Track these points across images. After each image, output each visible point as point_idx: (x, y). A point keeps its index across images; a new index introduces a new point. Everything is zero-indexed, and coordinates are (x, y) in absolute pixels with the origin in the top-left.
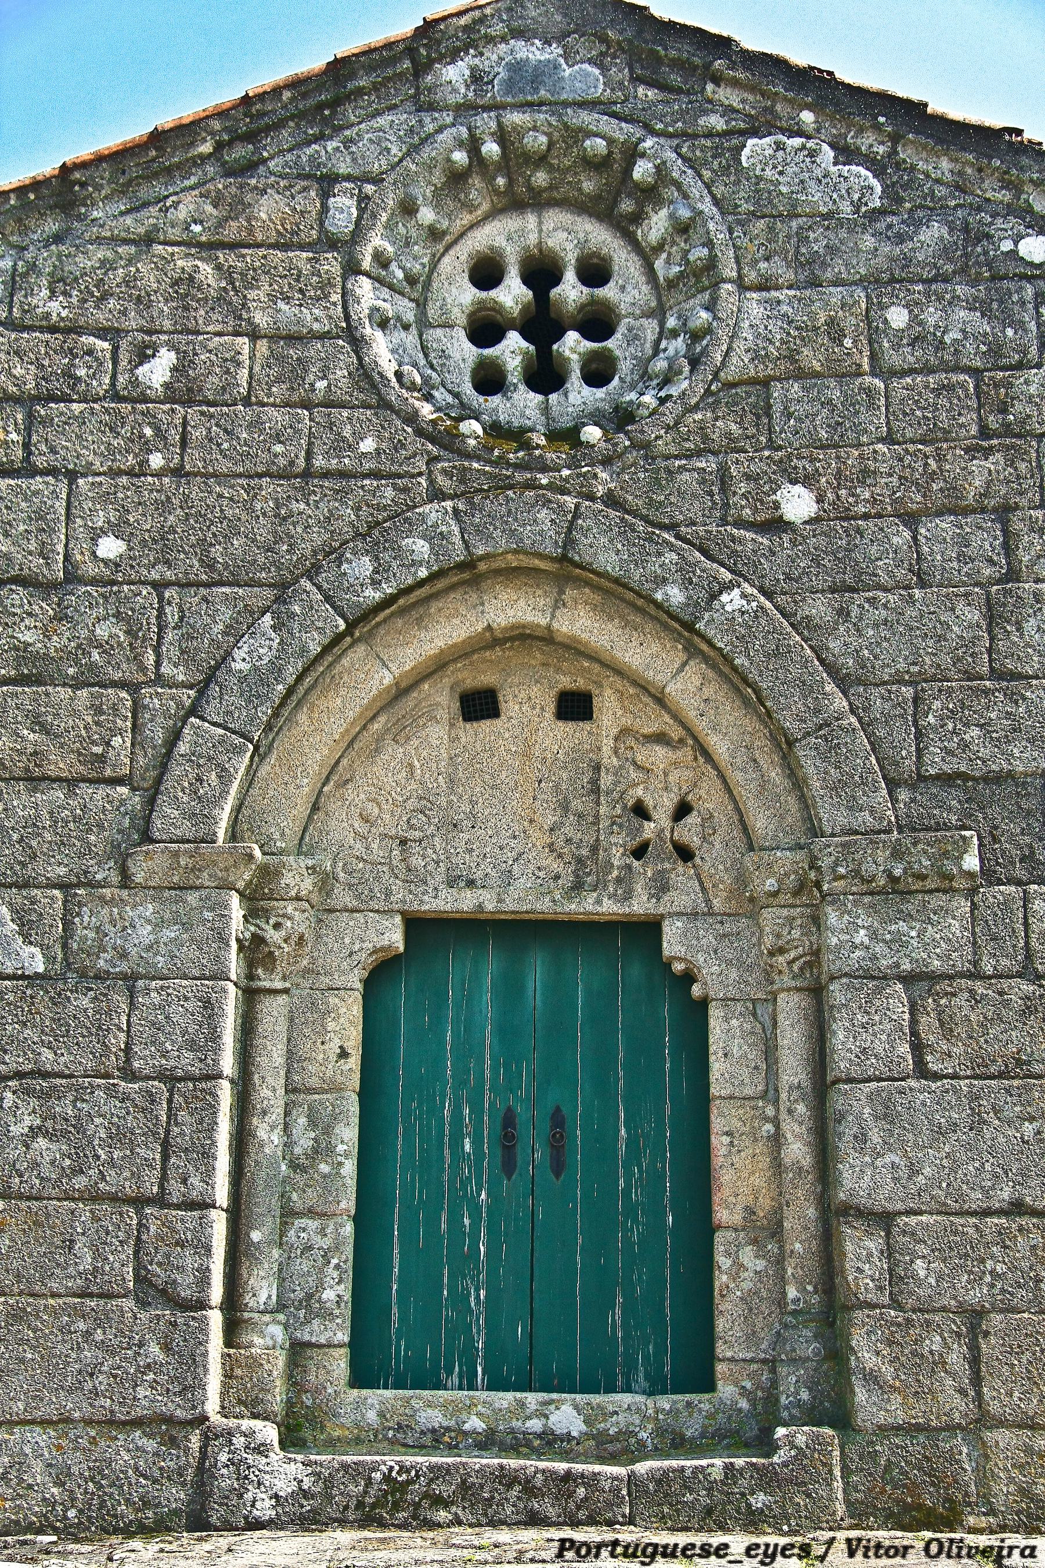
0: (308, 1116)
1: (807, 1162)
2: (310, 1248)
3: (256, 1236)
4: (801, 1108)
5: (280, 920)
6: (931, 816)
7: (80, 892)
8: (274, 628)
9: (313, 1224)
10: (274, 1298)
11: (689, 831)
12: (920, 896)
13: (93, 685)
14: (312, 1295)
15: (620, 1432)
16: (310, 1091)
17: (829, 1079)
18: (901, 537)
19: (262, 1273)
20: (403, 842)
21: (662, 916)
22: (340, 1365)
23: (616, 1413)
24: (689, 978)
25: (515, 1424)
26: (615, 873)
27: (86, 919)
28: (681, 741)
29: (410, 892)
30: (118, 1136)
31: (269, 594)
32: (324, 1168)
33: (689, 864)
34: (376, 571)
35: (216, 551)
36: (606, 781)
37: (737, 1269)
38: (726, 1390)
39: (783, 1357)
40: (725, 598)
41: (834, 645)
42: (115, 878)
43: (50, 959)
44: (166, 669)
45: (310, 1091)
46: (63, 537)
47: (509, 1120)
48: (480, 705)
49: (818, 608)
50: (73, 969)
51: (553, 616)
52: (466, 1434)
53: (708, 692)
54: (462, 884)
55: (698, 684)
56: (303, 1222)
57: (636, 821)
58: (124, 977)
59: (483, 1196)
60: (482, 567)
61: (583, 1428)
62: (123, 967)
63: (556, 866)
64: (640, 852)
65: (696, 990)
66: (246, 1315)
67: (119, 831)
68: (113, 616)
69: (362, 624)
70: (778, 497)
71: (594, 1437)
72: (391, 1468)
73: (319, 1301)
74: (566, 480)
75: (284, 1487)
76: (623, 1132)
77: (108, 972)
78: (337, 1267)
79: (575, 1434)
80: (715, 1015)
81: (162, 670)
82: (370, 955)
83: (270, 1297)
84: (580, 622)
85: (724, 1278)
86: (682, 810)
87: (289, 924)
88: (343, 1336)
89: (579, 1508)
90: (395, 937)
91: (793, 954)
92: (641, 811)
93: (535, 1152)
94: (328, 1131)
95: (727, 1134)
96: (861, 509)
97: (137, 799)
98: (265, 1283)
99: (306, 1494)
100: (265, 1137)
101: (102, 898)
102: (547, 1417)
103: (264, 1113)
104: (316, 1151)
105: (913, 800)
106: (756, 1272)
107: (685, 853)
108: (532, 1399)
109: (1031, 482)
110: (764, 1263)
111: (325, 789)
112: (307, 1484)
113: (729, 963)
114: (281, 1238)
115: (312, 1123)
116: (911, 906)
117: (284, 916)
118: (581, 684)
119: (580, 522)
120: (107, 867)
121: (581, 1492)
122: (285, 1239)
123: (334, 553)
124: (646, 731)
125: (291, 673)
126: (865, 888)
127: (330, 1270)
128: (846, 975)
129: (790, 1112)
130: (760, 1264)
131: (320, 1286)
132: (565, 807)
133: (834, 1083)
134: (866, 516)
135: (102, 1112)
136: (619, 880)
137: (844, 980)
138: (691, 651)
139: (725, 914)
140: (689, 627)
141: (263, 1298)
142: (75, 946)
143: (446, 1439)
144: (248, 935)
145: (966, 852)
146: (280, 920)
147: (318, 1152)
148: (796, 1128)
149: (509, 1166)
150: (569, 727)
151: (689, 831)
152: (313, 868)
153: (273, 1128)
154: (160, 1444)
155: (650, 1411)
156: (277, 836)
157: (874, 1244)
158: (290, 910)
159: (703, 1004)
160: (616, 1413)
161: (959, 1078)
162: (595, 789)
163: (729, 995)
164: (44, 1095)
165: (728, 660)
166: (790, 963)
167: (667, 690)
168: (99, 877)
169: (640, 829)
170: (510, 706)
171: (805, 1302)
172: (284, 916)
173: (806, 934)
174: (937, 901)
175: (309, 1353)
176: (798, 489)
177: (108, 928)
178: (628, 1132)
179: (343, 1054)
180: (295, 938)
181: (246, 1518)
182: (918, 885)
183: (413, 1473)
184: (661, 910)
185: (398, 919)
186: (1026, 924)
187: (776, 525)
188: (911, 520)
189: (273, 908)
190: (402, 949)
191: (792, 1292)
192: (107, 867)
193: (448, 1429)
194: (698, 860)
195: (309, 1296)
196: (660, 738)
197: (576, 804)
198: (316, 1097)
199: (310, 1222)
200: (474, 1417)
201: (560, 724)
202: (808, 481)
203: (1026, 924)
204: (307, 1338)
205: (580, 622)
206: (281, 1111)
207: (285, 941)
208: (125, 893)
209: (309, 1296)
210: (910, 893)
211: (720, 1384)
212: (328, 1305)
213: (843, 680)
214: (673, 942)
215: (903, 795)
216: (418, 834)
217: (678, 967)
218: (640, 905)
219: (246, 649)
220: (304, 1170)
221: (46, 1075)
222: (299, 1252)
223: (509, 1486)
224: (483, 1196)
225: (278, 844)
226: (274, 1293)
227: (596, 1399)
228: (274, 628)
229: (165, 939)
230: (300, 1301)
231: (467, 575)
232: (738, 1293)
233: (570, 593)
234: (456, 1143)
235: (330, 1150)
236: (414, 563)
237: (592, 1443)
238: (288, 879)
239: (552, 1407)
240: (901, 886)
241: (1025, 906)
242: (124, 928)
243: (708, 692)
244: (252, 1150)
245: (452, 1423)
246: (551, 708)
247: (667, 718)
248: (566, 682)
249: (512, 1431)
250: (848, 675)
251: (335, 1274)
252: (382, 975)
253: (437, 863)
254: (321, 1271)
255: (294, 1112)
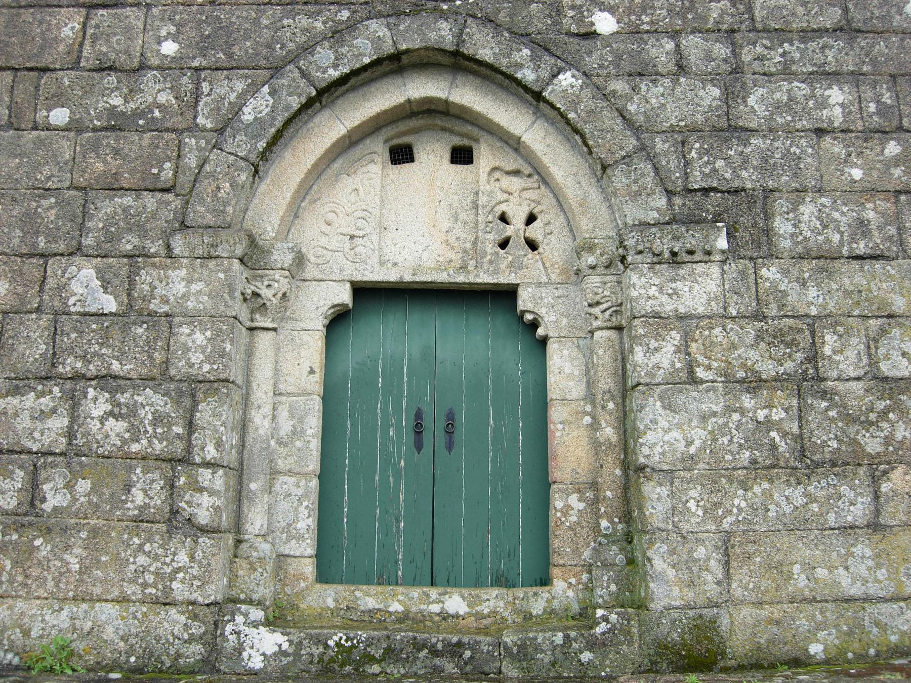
0: (289, 411)
1: (614, 439)
2: (290, 495)
3: (253, 486)
4: (611, 405)
5: (270, 282)
6: (694, 215)
7: (140, 260)
8: (270, 94)
9: (291, 480)
10: (265, 526)
11: (536, 231)
12: (690, 265)
13: (154, 131)
14: (291, 525)
15: (490, 612)
16: (289, 394)
17: (630, 383)
18: (670, 46)
19: (257, 510)
20: (352, 237)
21: (518, 285)
22: (309, 568)
23: (488, 600)
24: (534, 325)
25: (423, 607)
26: (489, 257)
27: (143, 277)
28: (530, 176)
29: (356, 269)
30: (158, 419)
31: (267, 73)
32: (298, 444)
33: (536, 252)
34: (337, 59)
35: (236, 49)
36: (483, 200)
37: (567, 506)
38: (559, 585)
39: (599, 564)
40: (561, 77)
41: (632, 108)
42: (163, 252)
43: (120, 304)
44: (200, 120)
45: (289, 394)
46: (141, 42)
47: (419, 415)
48: (402, 155)
49: (619, 86)
50: (133, 311)
51: (449, 93)
52: (390, 613)
53: (548, 141)
54: (390, 265)
55: (542, 135)
56: (286, 478)
57: (502, 225)
58: (167, 315)
59: (402, 463)
60: (405, 60)
61: (467, 610)
62: (166, 308)
63: (451, 255)
64: (504, 244)
65: (540, 332)
66: (246, 537)
67: (166, 222)
68: (169, 88)
69: (327, 95)
70: (593, 19)
71: (473, 615)
72: (341, 638)
73: (295, 529)
74: (459, 7)
75: (271, 649)
76: (491, 422)
77: (156, 312)
78: (307, 507)
79: (461, 613)
80: (552, 347)
81: (198, 121)
82: (329, 309)
83: (262, 525)
84: (468, 95)
85: (559, 514)
86: (531, 219)
87: (276, 285)
88: (310, 551)
89: (466, 664)
90: (345, 296)
91: (605, 306)
92: (503, 218)
93: (434, 435)
94: (301, 420)
95: (561, 423)
96: (646, 27)
97: (178, 202)
98: (259, 517)
99: (285, 654)
100: (259, 423)
101: (153, 265)
102: (443, 602)
103: (259, 407)
104: (294, 433)
105: (684, 205)
106: (579, 511)
107: (532, 245)
108: (434, 593)
109: (747, 16)
110: (584, 504)
111: (303, 204)
112: (285, 646)
113: (562, 314)
114: (271, 488)
115: (292, 416)
116: (683, 271)
117: (274, 280)
118: (466, 142)
119: (468, 30)
120: (157, 244)
121: (468, 654)
122: (273, 489)
123: (307, 49)
124: (507, 169)
125: (279, 123)
126: (655, 259)
127: (302, 509)
128: (643, 316)
129: (603, 407)
130: (582, 506)
131: (296, 520)
132: (456, 218)
133: (634, 387)
134: (648, 32)
135: (151, 401)
136: (491, 262)
137: (643, 319)
138: (538, 113)
139: (559, 283)
140: (538, 96)
141: (258, 526)
142: (136, 295)
143: (378, 616)
144: (249, 292)
145: (719, 236)
146: (270, 282)
147: (296, 433)
148: (607, 417)
149: (419, 446)
150: (460, 167)
151: (536, 231)
152: (292, 248)
153: (264, 417)
154: (188, 618)
155: (510, 599)
156: (269, 229)
157: (664, 491)
158: (277, 277)
159: (543, 342)
160: (488, 600)
161: (716, 382)
162: (476, 207)
163: (562, 335)
164: (113, 392)
165: (563, 116)
166: (604, 311)
167: (523, 139)
168: (152, 250)
169: (504, 230)
170: (420, 154)
171: (613, 529)
172: (274, 280)
173: (614, 293)
174: (700, 268)
175: (289, 560)
176: (606, 15)
177: (157, 283)
178: (495, 423)
179: (312, 371)
180: (280, 295)
181: (244, 667)
182: (688, 258)
183: (355, 641)
184: (518, 281)
185: (348, 285)
186: (756, 284)
187: (591, 35)
188: (675, 35)
189: (266, 275)
190: (351, 306)
191: (604, 523)
192: (157, 244)
193: (379, 610)
194: (541, 250)
195: (289, 525)
196: (516, 173)
197: (463, 216)
198: (294, 399)
199: (289, 478)
200: (396, 603)
201: (453, 166)
202: (611, 10)
203: (756, 284)
204: (287, 552)
205: (468, 95)
206: (270, 407)
207: (274, 296)
208: (169, 261)
209: (289, 525)
210: (684, 263)
211: (555, 581)
212: (301, 531)
213: (637, 129)
214: (525, 300)
215: (678, 201)
216: (361, 233)
217: (529, 317)
218: (505, 278)
219: (251, 107)
220: (286, 445)
221: (116, 377)
222: (282, 497)
223: (419, 650)
224: (402, 463)
225: (270, 234)
226: (266, 522)
227: (475, 592)
228: (270, 94)
229: (193, 291)
230: (283, 528)
231: (394, 64)
232: (568, 524)
233: (460, 79)
234: (385, 431)
235: (303, 432)
236: (360, 55)
237: (473, 619)
238: (275, 256)
239: (447, 596)
240: (679, 259)
241: (755, 273)
242: (168, 284)
243: (548, 141)
244: (251, 430)
245: (381, 606)
246: (447, 156)
247: (521, 161)
248: (457, 141)
249: (421, 612)
250: (641, 126)
251: (306, 512)
252: (338, 320)
253: (374, 250)
254: (296, 509)
255: (280, 408)
